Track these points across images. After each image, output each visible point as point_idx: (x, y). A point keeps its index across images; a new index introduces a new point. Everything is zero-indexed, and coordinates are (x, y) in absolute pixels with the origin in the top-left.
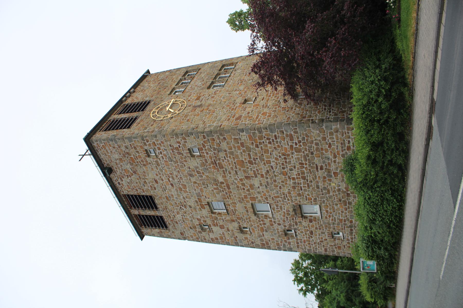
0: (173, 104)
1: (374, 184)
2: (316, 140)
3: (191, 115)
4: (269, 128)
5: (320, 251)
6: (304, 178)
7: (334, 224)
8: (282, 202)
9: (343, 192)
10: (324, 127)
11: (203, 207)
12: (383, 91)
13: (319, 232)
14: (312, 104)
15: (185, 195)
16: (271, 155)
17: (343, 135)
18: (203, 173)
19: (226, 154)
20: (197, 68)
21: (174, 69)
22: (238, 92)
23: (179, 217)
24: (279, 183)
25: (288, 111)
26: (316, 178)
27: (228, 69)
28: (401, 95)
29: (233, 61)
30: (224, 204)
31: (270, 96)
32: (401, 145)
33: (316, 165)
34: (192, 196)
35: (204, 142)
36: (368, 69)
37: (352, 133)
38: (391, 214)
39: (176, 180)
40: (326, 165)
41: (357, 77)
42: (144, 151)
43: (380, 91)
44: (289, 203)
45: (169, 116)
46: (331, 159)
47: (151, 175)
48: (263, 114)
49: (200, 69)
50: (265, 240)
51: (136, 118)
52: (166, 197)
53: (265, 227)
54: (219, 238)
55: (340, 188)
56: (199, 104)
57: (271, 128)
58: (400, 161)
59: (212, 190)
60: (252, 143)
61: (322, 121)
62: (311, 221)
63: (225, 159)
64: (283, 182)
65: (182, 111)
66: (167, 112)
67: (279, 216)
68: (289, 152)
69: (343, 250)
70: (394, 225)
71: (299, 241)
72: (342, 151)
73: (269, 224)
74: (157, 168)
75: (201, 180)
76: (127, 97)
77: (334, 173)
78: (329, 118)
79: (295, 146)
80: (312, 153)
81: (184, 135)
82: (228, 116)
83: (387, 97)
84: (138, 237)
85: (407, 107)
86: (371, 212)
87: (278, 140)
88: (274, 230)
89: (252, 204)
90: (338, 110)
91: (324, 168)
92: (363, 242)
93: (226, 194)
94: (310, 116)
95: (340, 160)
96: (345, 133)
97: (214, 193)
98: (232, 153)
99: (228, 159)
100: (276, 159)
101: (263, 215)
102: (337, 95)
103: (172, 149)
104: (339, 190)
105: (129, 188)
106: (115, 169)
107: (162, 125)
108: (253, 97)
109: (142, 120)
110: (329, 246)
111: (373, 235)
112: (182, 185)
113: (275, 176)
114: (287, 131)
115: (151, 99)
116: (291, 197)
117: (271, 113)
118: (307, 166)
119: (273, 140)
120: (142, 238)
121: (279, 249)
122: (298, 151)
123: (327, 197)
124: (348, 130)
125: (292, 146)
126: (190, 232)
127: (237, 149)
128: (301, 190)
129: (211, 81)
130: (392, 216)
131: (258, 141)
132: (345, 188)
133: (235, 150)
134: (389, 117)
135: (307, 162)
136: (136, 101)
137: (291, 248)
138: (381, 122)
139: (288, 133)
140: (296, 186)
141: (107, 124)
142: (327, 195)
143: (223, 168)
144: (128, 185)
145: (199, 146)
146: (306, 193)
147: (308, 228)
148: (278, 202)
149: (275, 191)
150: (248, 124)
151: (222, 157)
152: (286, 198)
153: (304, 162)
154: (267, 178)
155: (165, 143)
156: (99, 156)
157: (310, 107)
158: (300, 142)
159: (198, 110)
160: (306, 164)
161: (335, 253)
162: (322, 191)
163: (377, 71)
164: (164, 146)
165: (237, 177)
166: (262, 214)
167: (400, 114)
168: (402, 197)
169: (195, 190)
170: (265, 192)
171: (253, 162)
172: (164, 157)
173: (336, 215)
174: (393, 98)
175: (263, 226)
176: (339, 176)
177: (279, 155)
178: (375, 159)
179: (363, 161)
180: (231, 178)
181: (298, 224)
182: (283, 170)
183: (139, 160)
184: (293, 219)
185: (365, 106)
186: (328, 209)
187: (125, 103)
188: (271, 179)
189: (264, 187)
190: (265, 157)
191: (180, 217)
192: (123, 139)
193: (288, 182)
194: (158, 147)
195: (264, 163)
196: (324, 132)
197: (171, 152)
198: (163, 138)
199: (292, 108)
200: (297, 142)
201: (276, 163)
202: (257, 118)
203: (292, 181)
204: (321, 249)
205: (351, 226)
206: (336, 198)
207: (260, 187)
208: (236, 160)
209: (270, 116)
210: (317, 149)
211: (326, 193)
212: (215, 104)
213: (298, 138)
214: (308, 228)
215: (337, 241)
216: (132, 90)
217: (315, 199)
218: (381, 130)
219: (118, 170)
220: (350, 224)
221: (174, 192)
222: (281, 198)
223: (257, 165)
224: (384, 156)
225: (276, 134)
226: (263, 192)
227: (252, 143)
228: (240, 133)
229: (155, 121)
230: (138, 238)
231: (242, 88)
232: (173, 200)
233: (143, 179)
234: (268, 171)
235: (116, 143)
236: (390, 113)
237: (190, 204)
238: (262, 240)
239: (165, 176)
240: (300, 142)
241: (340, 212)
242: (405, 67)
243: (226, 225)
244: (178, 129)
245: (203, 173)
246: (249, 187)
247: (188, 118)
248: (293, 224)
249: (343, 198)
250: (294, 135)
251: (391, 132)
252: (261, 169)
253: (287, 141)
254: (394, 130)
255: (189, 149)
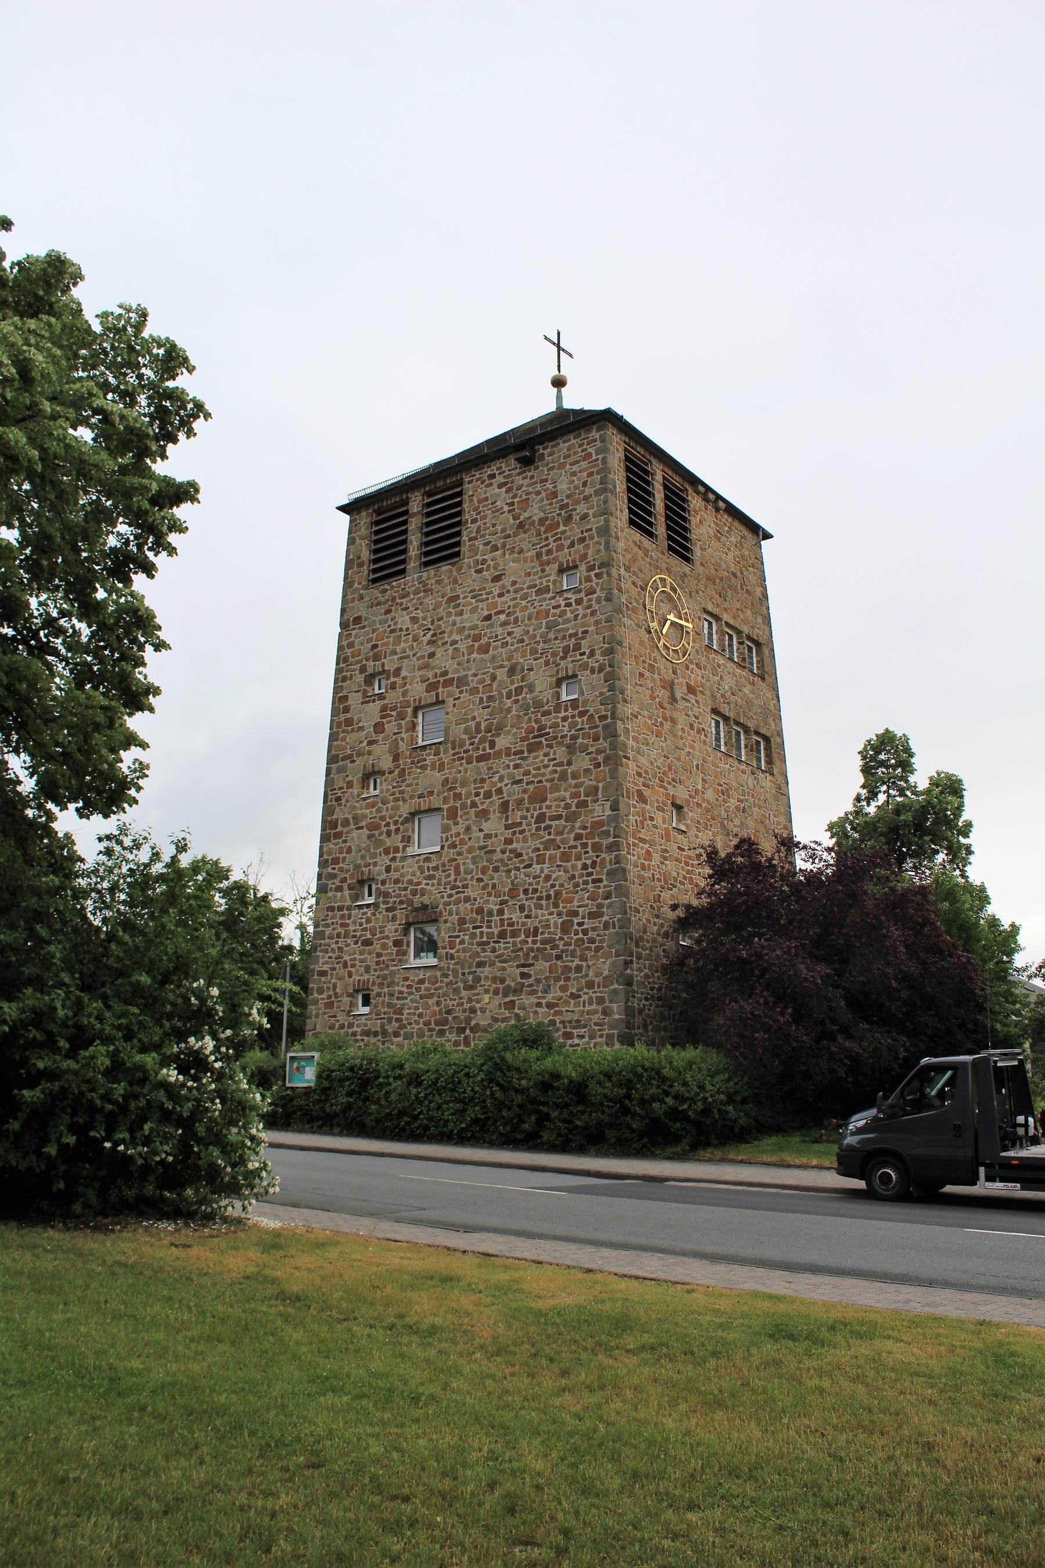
0: (682, 626)
1: (498, 1084)
2: (588, 967)
3: (653, 680)
4: (617, 869)
5: (321, 961)
6: (502, 935)
7: (391, 995)
8: (443, 880)
9: (468, 1020)
10: (616, 986)
11: (432, 687)
12: (686, 1106)
13: (371, 960)
14: (665, 961)
15: (462, 646)
16: (558, 866)
17: (596, 1024)
18: (517, 701)
19: (561, 764)
20: (766, 674)
21: (768, 609)
22: (700, 788)
23: (403, 620)
24: (492, 878)
25: (652, 907)
26: (500, 962)
27: (759, 752)
28: (677, 1139)
29: (778, 763)
30: (440, 743)
31: (687, 864)
32: (578, 1137)
33: (533, 965)
34: (459, 664)
35: (592, 716)
36: (728, 1081)
37: (600, 1044)
38: (431, 1119)
39: (500, 630)
40: (531, 985)
41: (714, 1058)
42: (574, 561)
43: (684, 1100)
44: (442, 897)
45: (654, 625)
46: (544, 998)
47: (513, 568)
48: (648, 852)
49: (763, 679)
50: (345, 830)
51: (650, 534)
52: (457, 597)
53: (381, 834)
54: (349, 715)
55: (479, 1013)
56: (678, 695)
57: (618, 873)
58: (546, 1136)
59: (474, 718)
60: (585, 828)
61: (629, 983)
62: (397, 943)
63: (549, 760)
64: (494, 886)
65: (662, 655)
66: (663, 614)
67: (409, 870)
68: (564, 907)
69: (325, 1013)
70: (407, 1123)
71: (345, 912)
72: (561, 1022)
73: (388, 845)
74: (529, 587)
75: (501, 694)
76: (706, 493)
77: (513, 1002)
78: (634, 997)
79: (576, 921)
80: (559, 957)
81: (608, 669)
82: (646, 772)
83: (674, 1113)
84: (346, 502)
85: (653, 1149)
86: (437, 1079)
87: (591, 885)
88: (374, 855)
89: (440, 809)
90: (649, 1016)
91: (526, 982)
92: (362, 1059)
93: (466, 751)
94: (639, 957)
95: (543, 1015)
96: (600, 1030)
97: (466, 720)
98: (563, 777)
99: (551, 768)
100: (548, 878)
101: (410, 833)
102: (681, 1013)
103: (576, 634)
104: (473, 1010)
105: (479, 502)
106: (529, 474)
107: (634, 610)
108: (687, 825)
109: (646, 552)
110: (333, 981)
111: (381, 1080)
112: (489, 644)
113: (509, 871)
114: (609, 906)
115: (697, 563)
116: (457, 902)
117: (649, 869)
118: (530, 945)
119: (591, 874)
120: (343, 509)
121: (323, 864)
122: (566, 928)
123: (456, 982)
124: (609, 1036)
125: (575, 914)
126: (362, 644)
127: (573, 790)
128: (475, 928)
129: (732, 715)
130: (428, 1119)
131: (590, 842)
132: (477, 1025)
133: (571, 786)
134: (634, 1115)
135: (538, 945)
136: (694, 520)
137: (326, 892)
138: (627, 1101)
139: (605, 910)
140: (483, 917)
141: (642, 454)
142: (461, 985)
143: (530, 751)
144: (486, 499)
145: (583, 702)
146: (467, 938)
147: (378, 935)
148: (443, 871)
149: (471, 866)
150: (628, 820)
151: (555, 754)
152: (453, 892)
153: (539, 937)
154: (503, 852)
155: (592, 620)
156: (565, 438)
157: (658, 955)
158: (585, 932)
159: (663, 694)
160: (534, 942)
161: (316, 995)
162: (470, 973)
163: (722, 1097)
164: (584, 616)
165: (506, 781)
166: (413, 831)
167: (640, 1136)
168: (468, 1139)
169: (475, 675)
170: (470, 844)
171: (543, 825)
172: (557, 611)
173: (412, 1001)
174: (671, 1123)
175: (384, 829)
176: (507, 1013)
177: (557, 883)
178: (552, 1087)
179: (548, 1063)
180: (503, 766)
181: (390, 914)
182: (521, 889)
183: (553, 545)
184: (401, 902)
185: (658, 1072)
186: (426, 985)
187: (690, 491)
188: (501, 861)
189: (482, 844)
190: (552, 852)
191: (403, 623)
192: (606, 512)
193: (492, 898)
194: (582, 599)
195: (538, 850)
196: (604, 987)
197: (571, 631)
198: (603, 617)
199: (657, 916)
200: (585, 927)
201: (539, 876)
202: (641, 840)
203: (495, 908)
204: (327, 963)
205: (384, 1033)
206: (455, 1003)
207: (481, 835)
208: (548, 785)
209: (643, 868)
210: (567, 969)
211: (465, 982)
212: (675, 736)
213: (594, 929)
214: (378, 935)
215: (346, 999)
216: (721, 504)
217: (452, 957)
218: (610, 1100)
219: (527, 481)
220: (390, 1030)
221: (470, 619)
222: (455, 880)
223: (534, 831)
224: (557, 1106)
225: (605, 883)
226: (470, 839)
227: (585, 828)
228: (609, 803)
229: (643, 589)
230: (345, 501)
231: (710, 795)
232: (449, 614)
233: (504, 546)
234: (520, 855)
235: (598, 493)
236: (643, 1118)
237: (438, 655)
238: (346, 823)
239: (511, 603)
240: (585, 932)
241: (421, 1010)
242: (727, 1148)
243: (384, 739)
244: (623, 655)
245: (517, 701)
246: (481, 808)
247: (647, 674)
248: (388, 902)
249: (454, 1018)
250: (600, 922)
251: (606, 1119)
252: (525, 840)
253: (587, 905)
254: (610, 1126)
255: (575, 676)
